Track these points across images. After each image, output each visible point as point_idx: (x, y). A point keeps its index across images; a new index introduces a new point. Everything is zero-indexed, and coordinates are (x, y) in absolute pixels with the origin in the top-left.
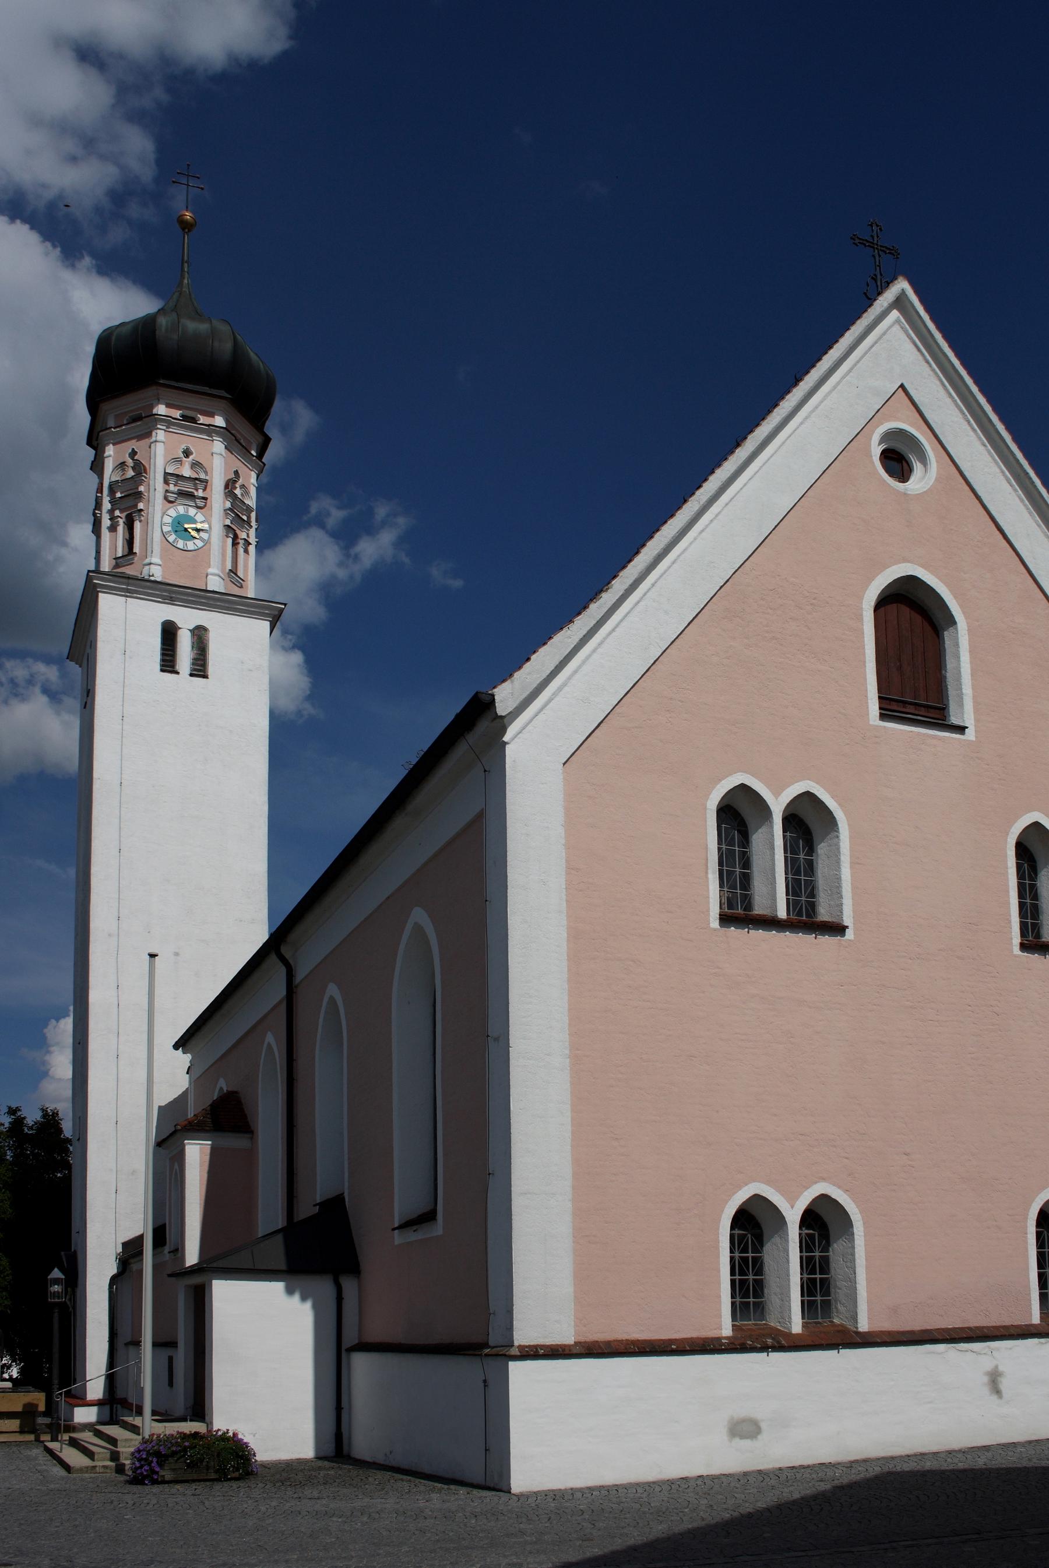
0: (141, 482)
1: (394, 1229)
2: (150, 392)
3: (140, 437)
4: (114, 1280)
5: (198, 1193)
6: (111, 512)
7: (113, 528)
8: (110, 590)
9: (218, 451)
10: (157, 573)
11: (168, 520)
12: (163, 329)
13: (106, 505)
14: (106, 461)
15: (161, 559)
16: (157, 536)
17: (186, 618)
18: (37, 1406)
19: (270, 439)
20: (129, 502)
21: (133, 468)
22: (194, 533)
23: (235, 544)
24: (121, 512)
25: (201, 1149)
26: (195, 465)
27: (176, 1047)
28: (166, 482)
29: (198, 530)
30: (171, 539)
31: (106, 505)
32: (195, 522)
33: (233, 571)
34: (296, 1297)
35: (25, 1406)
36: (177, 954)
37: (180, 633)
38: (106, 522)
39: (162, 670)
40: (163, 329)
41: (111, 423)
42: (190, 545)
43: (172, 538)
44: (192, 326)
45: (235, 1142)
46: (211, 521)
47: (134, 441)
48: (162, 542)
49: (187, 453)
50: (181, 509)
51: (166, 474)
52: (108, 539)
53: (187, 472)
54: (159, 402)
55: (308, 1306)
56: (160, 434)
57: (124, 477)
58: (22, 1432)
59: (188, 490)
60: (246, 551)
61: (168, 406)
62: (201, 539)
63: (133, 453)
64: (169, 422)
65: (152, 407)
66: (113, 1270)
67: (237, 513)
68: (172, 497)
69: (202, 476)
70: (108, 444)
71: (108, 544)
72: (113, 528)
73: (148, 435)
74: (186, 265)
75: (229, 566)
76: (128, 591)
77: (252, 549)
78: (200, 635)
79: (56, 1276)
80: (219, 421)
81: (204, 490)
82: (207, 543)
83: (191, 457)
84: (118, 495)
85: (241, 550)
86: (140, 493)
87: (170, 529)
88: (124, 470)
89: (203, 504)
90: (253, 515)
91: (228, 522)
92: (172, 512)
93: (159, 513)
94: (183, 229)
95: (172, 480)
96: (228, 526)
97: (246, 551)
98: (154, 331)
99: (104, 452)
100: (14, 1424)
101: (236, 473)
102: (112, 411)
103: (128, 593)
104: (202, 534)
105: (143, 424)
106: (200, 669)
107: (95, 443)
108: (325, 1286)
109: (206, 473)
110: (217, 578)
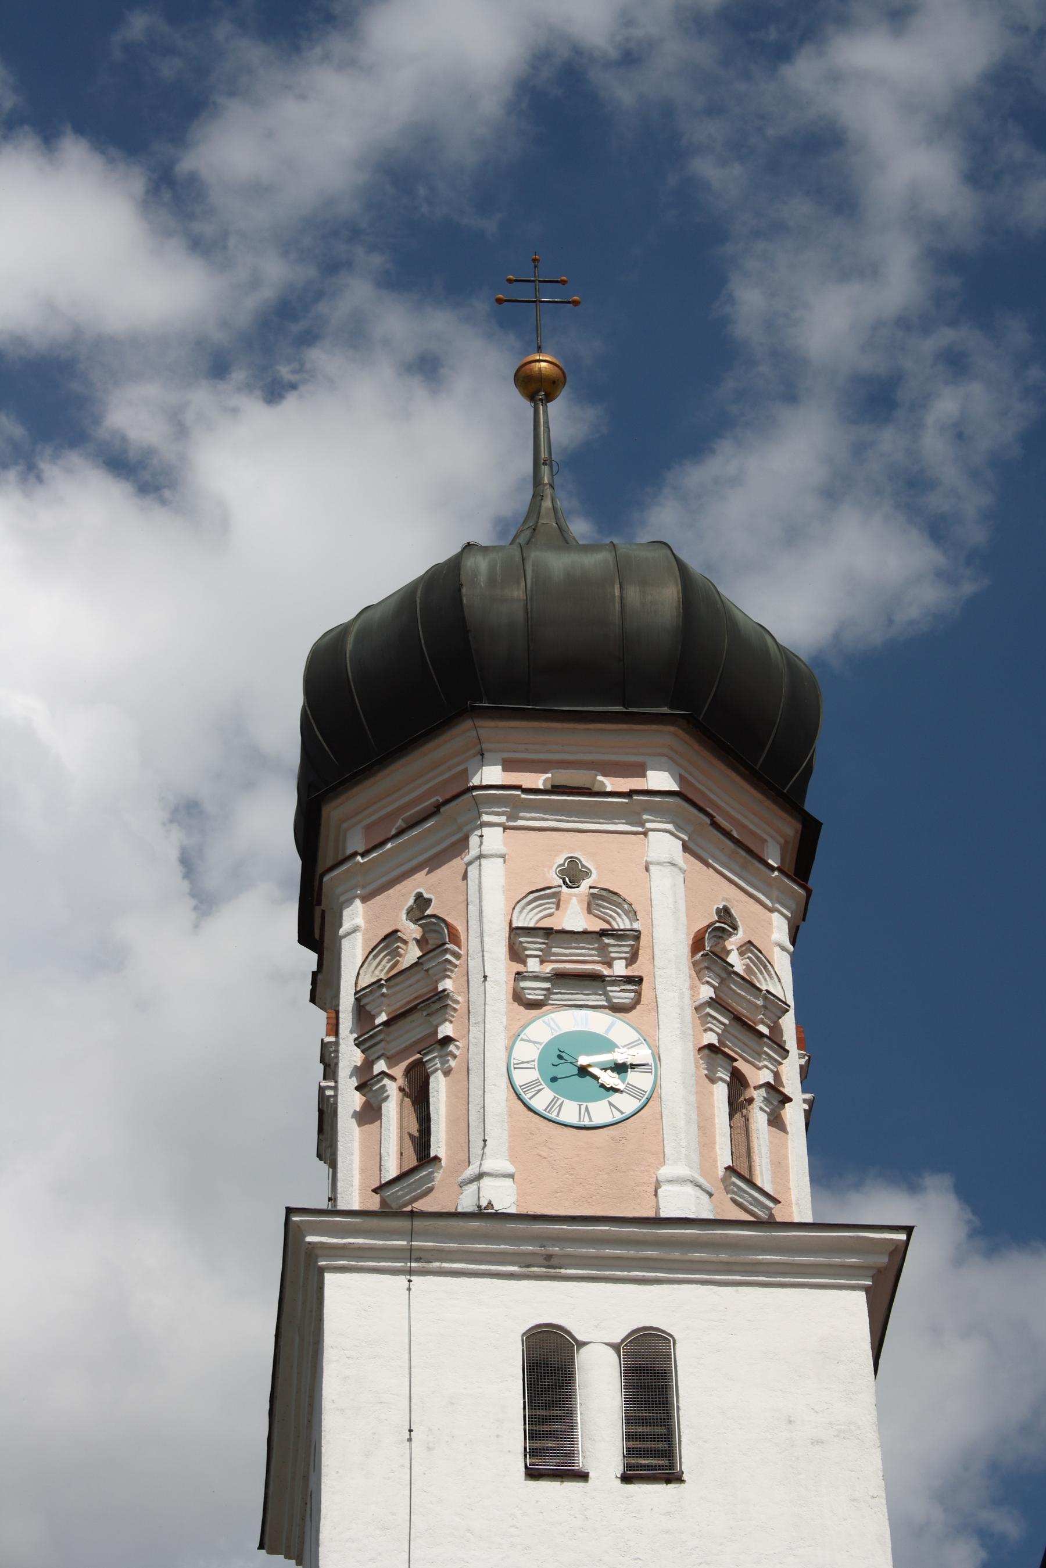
3: (434, 862)
7: (370, 1114)
8: (357, 1260)
9: (664, 857)
10: (503, 1197)
11: (527, 1052)
12: (482, 579)
13: (350, 1056)
14: (345, 944)
15: (513, 1158)
16: (497, 1099)
17: (600, 1314)
19: (818, 825)
20: (412, 1030)
22: (609, 1078)
23: (738, 1104)
24: (392, 1061)
28: (516, 954)
29: (620, 1068)
30: (540, 1102)
31: (350, 1056)
32: (611, 1046)
33: (740, 1173)
37: (583, 1359)
38: (350, 1100)
39: (533, 1474)
41: (356, 842)
42: (600, 1112)
46: (668, 1027)
47: (421, 876)
48: (511, 1113)
49: (573, 874)
51: (515, 932)
53: (574, 916)
54: (482, 757)
56: (492, 838)
60: (776, 1122)
61: (508, 766)
62: (633, 1091)
64: (514, 803)
65: (465, 775)
67: (736, 1026)
68: (534, 990)
69: (622, 923)
70: (350, 901)
72: (370, 1114)
73: (462, 845)
74: (545, 470)
75: (724, 1158)
76: (412, 1254)
77: (794, 1114)
78: (649, 1373)
83: (585, 884)
85: (759, 1119)
86: (444, 995)
87: (534, 1075)
88: (395, 953)
89: (628, 995)
90: (788, 1024)
91: (711, 1038)
93: (501, 1039)
94: (532, 397)
95: (533, 946)
96: (710, 1047)
97: (776, 1122)
98: (463, 619)
101: (725, 913)
102: (351, 818)
103: (413, 1262)
104: (632, 1076)
105: (445, 822)
106: (652, 1452)
109: (633, 915)
110: (689, 1189)
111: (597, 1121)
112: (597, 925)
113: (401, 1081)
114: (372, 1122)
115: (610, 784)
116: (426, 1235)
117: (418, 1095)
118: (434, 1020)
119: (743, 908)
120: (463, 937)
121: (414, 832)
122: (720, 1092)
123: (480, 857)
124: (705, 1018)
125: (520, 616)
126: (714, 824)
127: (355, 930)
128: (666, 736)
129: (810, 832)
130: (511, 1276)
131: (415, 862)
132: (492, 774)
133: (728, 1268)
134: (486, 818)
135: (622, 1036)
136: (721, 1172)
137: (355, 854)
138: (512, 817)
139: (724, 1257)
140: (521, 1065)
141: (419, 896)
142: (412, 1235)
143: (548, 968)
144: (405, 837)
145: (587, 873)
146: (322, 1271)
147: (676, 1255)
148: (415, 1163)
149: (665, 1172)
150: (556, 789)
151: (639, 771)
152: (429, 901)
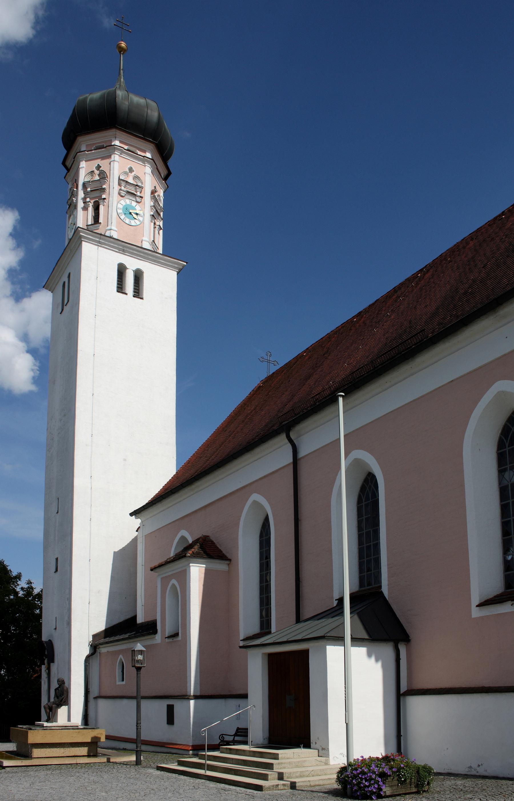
0: (105, 183)
1: (166, 638)
2: (112, 132)
3: (103, 158)
4: (88, 659)
5: (198, 599)
6: (84, 199)
7: (85, 209)
8: (89, 240)
10: (115, 235)
11: (120, 206)
12: (120, 97)
15: (117, 227)
16: (115, 214)
17: (132, 264)
18: (100, 738)
20: (96, 194)
21: (99, 175)
24: (91, 199)
25: (199, 569)
26: (136, 177)
27: (131, 514)
28: (120, 185)
29: (137, 214)
30: (123, 217)
33: (154, 241)
34: (373, 659)
35: (92, 738)
36: (125, 460)
37: (127, 271)
40: (120, 97)
41: (83, 148)
42: (133, 223)
43: (123, 217)
44: (136, 99)
45: (220, 566)
46: (145, 209)
47: (99, 160)
49: (131, 170)
50: (128, 202)
52: (82, 215)
53: (131, 180)
55: (379, 664)
56: (116, 157)
57: (92, 180)
58: (89, 756)
59: (132, 191)
61: (121, 142)
62: (139, 220)
63: (98, 167)
64: (122, 151)
65: (111, 141)
66: (87, 651)
69: (140, 184)
70: (82, 161)
71: (82, 217)
72: (85, 209)
73: (109, 157)
76: (99, 242)
78: (138, 277)
79: (140, 649)
80: (149, 155)
81: (141, 193)
82: (142, 223)
83: (133, 173)
84: (89, 189)
85: (157, 232)
88: (92, 176)
92: (122, 202)
99: (79, 165)
100: (84, 751)
101: (155, 187)
102: (83, 143)
103: (99, 244)
105: (105, 150)
106: (138, 293)
107: (68, 163)
108: (388, 650)
109: (142, 183)
111: (132, 224)
112: (136, 184)
113: (92, 204)
114: (85, 210)
115: (139, 153)
116: (103, 239)
117: (96, 208)
118: (102, 193)
119: (158, 188)
120: (109, 177)
121: (100, 150)
122: (153, 224)
123: (114, 161)
124: (152, 209)
125: (127, 109)
126: (157, 168)
127: (83, 167)
128: (151, 146)
129: (169, 173)
130: (116, 252)
131: (98, 157)
132: (117, 143)
133: (154, 261)
134: (116, 152)
135: (138, 209)
136: (151, 241)
137: (85, 151)
138: (121, 154)
139: (154, 259)
140: (119, 208)
141: (98, 165)
142: (100, 239)
143: (125, 189)
144: (97, 151)
145: (134, 171)
146: (82, 241)
147: (146, 256)
148: (93, 223)
149: (144, 238)
150: (128, 150)
151: (145, 152)
152: (101, 167)
